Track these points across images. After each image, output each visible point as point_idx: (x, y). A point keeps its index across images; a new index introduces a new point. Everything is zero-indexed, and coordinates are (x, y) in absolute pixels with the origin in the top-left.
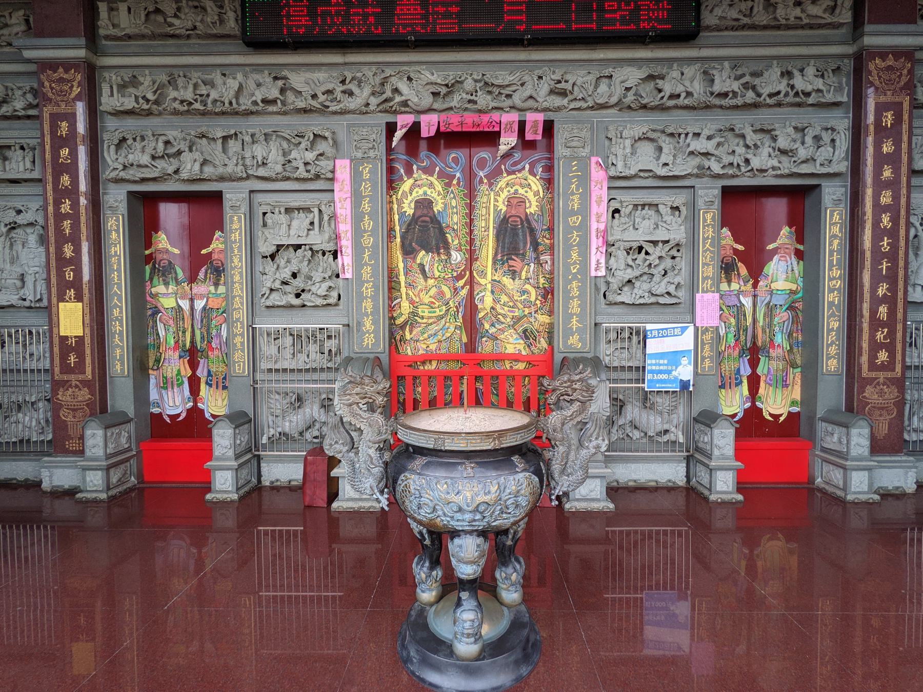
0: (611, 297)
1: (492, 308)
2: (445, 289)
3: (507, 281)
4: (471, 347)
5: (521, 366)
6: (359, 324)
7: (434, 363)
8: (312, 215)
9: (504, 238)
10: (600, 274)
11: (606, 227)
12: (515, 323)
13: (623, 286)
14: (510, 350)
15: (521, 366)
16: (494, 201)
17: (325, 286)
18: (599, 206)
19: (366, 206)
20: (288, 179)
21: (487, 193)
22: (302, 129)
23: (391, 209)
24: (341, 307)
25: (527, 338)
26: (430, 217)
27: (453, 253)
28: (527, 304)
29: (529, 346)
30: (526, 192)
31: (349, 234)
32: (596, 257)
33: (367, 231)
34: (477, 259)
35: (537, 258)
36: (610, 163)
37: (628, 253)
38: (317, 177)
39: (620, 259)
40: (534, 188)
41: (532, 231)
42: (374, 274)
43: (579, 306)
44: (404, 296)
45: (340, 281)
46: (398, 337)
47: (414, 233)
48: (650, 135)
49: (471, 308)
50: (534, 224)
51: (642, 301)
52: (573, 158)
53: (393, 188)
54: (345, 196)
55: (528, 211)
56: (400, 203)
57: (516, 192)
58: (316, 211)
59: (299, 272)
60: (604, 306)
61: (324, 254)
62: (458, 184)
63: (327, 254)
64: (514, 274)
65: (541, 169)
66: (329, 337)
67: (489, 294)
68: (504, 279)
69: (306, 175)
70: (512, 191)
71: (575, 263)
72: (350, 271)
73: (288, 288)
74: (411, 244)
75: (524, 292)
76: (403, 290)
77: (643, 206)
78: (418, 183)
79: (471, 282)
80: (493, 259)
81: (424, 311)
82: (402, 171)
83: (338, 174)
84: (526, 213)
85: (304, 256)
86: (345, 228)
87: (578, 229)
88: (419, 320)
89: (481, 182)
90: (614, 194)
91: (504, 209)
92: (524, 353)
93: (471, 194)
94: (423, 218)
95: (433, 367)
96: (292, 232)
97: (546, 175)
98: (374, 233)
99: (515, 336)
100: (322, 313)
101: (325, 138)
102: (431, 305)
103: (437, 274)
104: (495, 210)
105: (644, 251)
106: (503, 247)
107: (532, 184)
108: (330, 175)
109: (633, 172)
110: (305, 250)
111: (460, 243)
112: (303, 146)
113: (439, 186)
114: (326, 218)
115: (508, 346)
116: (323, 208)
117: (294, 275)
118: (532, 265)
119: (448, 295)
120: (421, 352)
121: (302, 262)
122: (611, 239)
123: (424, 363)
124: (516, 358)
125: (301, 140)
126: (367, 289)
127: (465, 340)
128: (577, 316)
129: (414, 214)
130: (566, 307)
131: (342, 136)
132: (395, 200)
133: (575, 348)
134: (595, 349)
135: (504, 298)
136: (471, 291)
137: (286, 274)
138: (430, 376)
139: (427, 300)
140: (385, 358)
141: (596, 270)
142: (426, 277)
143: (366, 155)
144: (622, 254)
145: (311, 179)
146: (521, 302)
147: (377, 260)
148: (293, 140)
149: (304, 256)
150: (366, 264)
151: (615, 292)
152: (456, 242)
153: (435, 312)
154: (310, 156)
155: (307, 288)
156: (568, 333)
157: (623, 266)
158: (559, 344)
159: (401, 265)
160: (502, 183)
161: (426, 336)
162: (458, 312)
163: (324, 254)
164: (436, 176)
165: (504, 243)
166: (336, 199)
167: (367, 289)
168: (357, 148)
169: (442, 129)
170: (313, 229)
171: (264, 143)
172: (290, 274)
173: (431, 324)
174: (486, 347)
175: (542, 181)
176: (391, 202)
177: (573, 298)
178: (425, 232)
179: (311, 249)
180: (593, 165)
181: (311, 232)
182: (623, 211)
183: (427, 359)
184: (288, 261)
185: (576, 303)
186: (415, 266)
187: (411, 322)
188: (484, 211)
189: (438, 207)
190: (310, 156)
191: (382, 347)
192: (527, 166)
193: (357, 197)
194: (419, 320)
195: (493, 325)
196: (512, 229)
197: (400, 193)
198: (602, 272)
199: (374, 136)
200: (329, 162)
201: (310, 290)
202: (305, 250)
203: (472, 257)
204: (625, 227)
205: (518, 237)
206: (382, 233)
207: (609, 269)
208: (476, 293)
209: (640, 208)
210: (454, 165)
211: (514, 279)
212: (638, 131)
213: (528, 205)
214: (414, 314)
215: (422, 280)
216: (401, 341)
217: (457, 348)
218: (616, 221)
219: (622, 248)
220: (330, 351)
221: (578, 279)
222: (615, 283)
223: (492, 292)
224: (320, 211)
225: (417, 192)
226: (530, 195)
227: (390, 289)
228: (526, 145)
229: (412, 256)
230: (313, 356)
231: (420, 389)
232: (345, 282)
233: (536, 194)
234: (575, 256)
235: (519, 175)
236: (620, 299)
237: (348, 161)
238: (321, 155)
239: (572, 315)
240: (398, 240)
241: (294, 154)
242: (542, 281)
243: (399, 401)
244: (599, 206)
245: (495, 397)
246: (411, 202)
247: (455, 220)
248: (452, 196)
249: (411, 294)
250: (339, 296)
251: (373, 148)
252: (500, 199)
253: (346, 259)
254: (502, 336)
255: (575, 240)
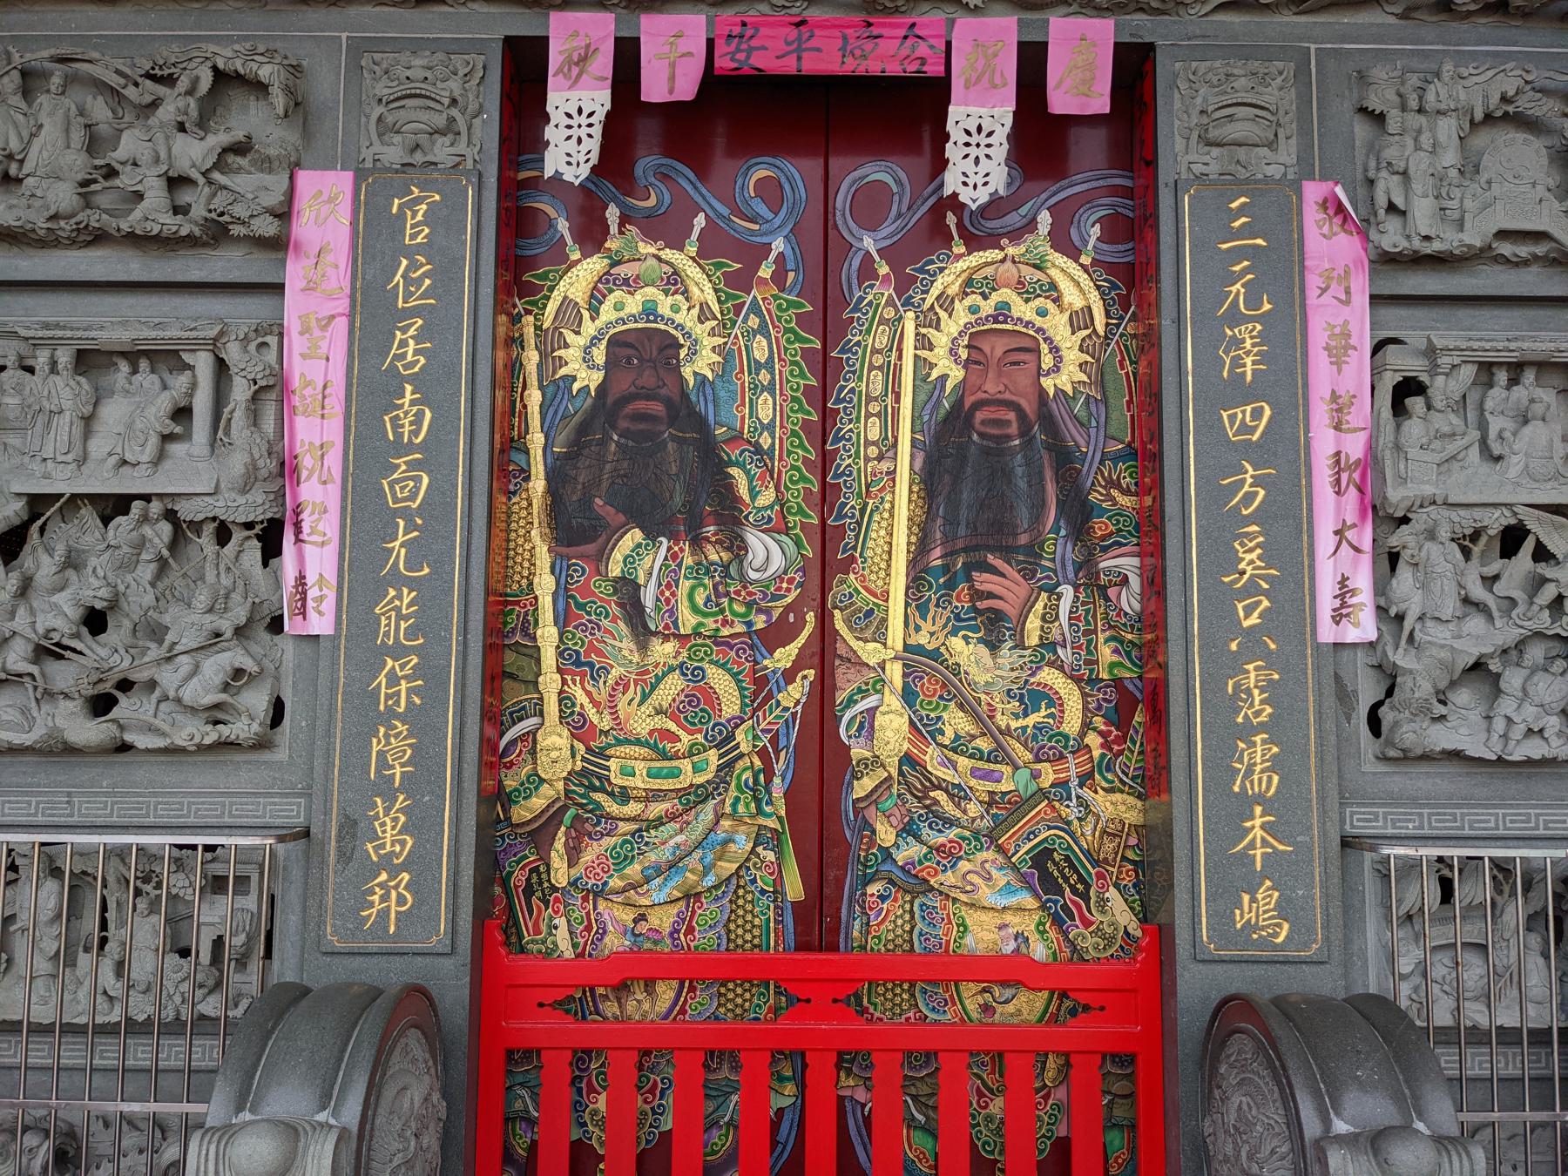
0: (1411, 732)
1: (908, 759)
2: (719, 680)
3: (965, 651)
4: (818, 921)
5: (1025, 1006)
6: (353, 829)
7: (666, 992)
8: (183, 380)
9: (957, 480)
10: (1352, 635)
11: (1371, 448)
12: (1000, 825)
13: (1453, 684)
14: (983, 935)
15: (1025, 1006)
16: (919, 345)
17: (216, 666)
18: (1338, 364)
19: (409, 349)
20: (99, 238)
21: (890, 313)
22: (170, 53)
23: (515, 367)
24: (281, 755)
25: (1049, 885)
26: (668, 403)
27: (757, 542)
28: (1049, 746)
29: (1057, 922)
30: (1042, 313)
31: (334, 460)
32: (1340, 566)
33: (411, 448)
34: (847, 565)
35: (1087, 566)
36: (1382, 202)
37: (1467, 553)
38: (217, 233)
39: (1438, 577)
40: (1073, 298)
41: (1065, 460)
42: (426, 622)
43: (1276, 765)
44: (552, 706)
45: (286, 649)
46: (519, 878)
47: (602, 460)
48: (1528, 104)
49: (821, 753)
50: (1074, 435)
51: (1535, 749)
52: (1231, 183)
53: (527, 290)
54: (329, 308)
55: (1048, 383)
56: (550, 344)
57: (1002, 313)
58: (203, 363)
59: (114, 604)
60: (1370, 766)
61: (223, 534)
62: (779, 277)
63: (238, 535)
64: (994, 627)
65: (1096, 231)
66: (217, 884)
67: (893, 701)
68: (957, 643)
69: (167, 222)
70: (987, 308)
71: (1251, 589)
72: (329, 605)
73: (62, 674)
74: (586, 503)
75: (1032, 698)
76: (550, 682)
77: (1516, 370)
78: (623, 270)
79: (824, 654)
80: (912, 564)
81: (630, 769)
82: (563, 226)
83: (305, 226)
84: (1042, 392)
85: (141, 544)
86: (318, 434)
87: (1259, 453)
88: (612, 807)
89: (867, 271)
90: (1398, 321)
91: (957, 374)
92: (1039, 951)
93: (828, 319)
94: (641, 405)
95: (663, 1005)
96: (99, 446)
97: (1118, 253)
98: (434, 456)
99: (1001, 877)
100: (202, 778)
101: (261, 88)
102: (659, 746)
103: (688, 620)
104: (920, 378)
105: (1528, 546)
106: (951, 522)
107: (1064, 285)
108: (266, 227)
109: (1474, 236)
110: (145, 518)
111: (780, 501)
112: (167, 112)
113: (703, 289)
114: (240, 392)
115: (972, 918)
116: (232, 353)
117: (95, 621)
118: (1067, 591)
119: (731, 705)
120: (614, 942)
121: (129, 565)
122: (1397, 496)
123: (621, 988)
124: (1008, 971)
125: (161, 90)
126: (393, 680)
127: (794, 888)
128: (1269, 805)
129: (602, 388)
130: (1221, 770)
131: (327, 82)
132: (529, 332)
133: (1265, 943)
134: (1347, 942)
135: (956, 722)
136: (823, 691)
137: (57, 613)
138: (645, 1051)
139: (642, 722)
140: (453, 984)
141: (1337, 618)
142: (643, 634)
143: (418, 158)
144: (1442, 557)
145: (191, 242)
146: (1022, 736)
147: (441, 567)
148: (131, 92)
149: (141, 544)
150: (396, 580)
151: (1424, 710)
152: (767, 497)
153: (675, 774)
154: (192, 152)
155: (139, 676)
156: (1235, 877)
157: (1450, 606)
158: (1196, 921)
159: (545, 584)
160: (948, 279)
161: (634, 870)
162: (769, 772)
163: (223, 534)
164: (692, 250)
165: (953, 504)
166: (291, 321)
167: (393, 680)
168: (385, 129)
169: (723, 63)
170: (186, 436)
171: (17, 100)
172: (75, 613)
173: (659, 822)
174: (880, 921)
175: (1101, 274)
176: (515, 342)
177: (1247, 731)
178: (645, 456)
179: (170, 515)
180: (1313, 218)
181: (176, 449)
182: (1441, 388)
183: (636, 970)
184: (73, 562)
185: (1259, 751)
186: (601, 589)
187: (580, 811)
188: (877, 381)
189: (700, 364)
190: (192, 152)
191: (447, 924)
192: (1045, 219)
193: (371, 315)
194: (612, 807)
195: (908, 830)
196: (987, 452)
197: (552, 307)
198: (1363, 627)
199: (455, 85)
200: (268, 179)
201: (152, 685)
202: (145, 518)
203: (830, 555)
204: (1452, 448)
205: (1002, 482)
206: (467, 456)
207: (1389, 616)
208: (841, 697)
209: (1502, 377)
210: (762, 209)
211: (993, 647)
212: (1481, 88)
213: (1047, 361)
214: (590, 778)
215: (627, 645)
216: (529, 891)
217: (765, 927)
218: (1414, 428)
219: (1444, 533)
220: (218, 943)
221: (1267, 655)
222: (1418, 674)
223: (908, 696)
224: (221, 366)
225: (619, 306)
226: (1058, 325)
227: (495, 677)
228: (1039, 139)
229: (590, 548)
230: (143, 966)
231: (601, 1103)
232: (307, 648)
233: (1081, 319)
234: (1250, 559)
235: (1011, 251)
236: (1442, 738)
237: (347, 177)
238: (240, 148)
239: (1245, 804)
240: (538, 485)
241: (130, 144)
242: (1106, 653)
243: (508, 1157)
244: (1338, 364)
245: (919, 1138)
246: (594, 341)
247: (765, 412)
248: (754, 322)
249: (581, 697)
250: (278, 709)
251: (450, 129)
252: (941, 340)
253: (315, 558)
254: (949, 878)
255: (1250, 497)
